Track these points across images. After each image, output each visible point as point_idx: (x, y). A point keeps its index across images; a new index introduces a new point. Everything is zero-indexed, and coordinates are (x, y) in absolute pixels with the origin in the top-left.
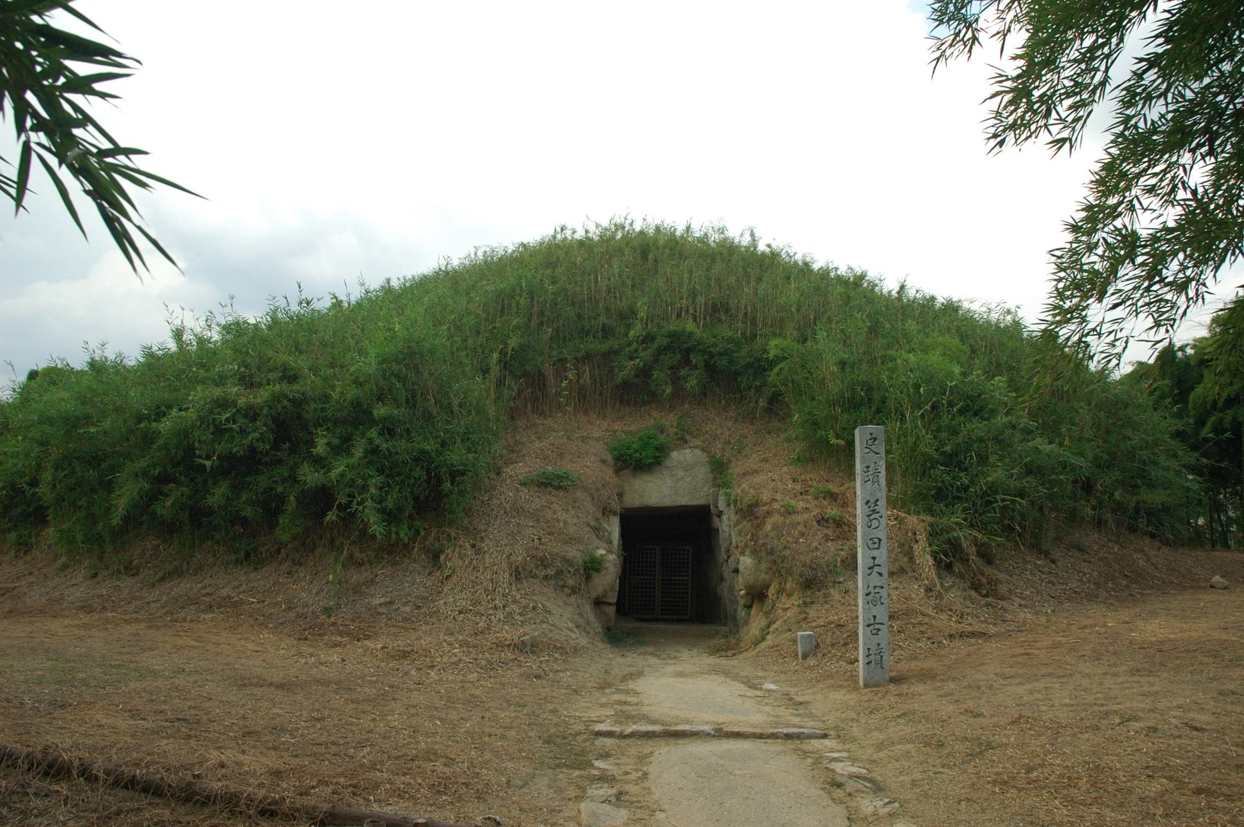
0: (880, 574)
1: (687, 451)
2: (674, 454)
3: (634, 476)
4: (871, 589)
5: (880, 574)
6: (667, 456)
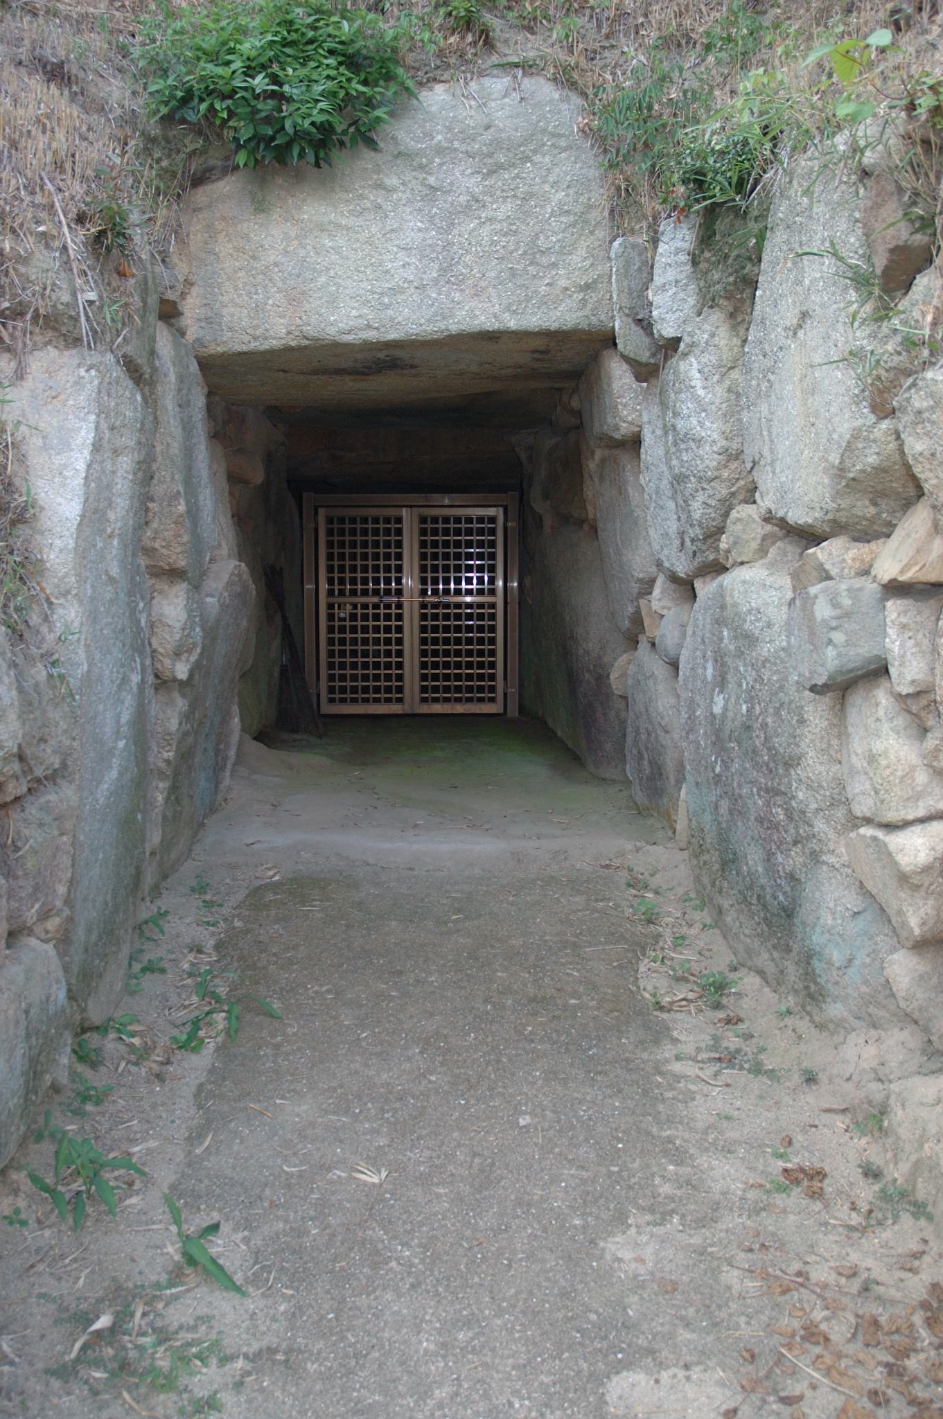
2: (436, 97)
3: (260, 207)
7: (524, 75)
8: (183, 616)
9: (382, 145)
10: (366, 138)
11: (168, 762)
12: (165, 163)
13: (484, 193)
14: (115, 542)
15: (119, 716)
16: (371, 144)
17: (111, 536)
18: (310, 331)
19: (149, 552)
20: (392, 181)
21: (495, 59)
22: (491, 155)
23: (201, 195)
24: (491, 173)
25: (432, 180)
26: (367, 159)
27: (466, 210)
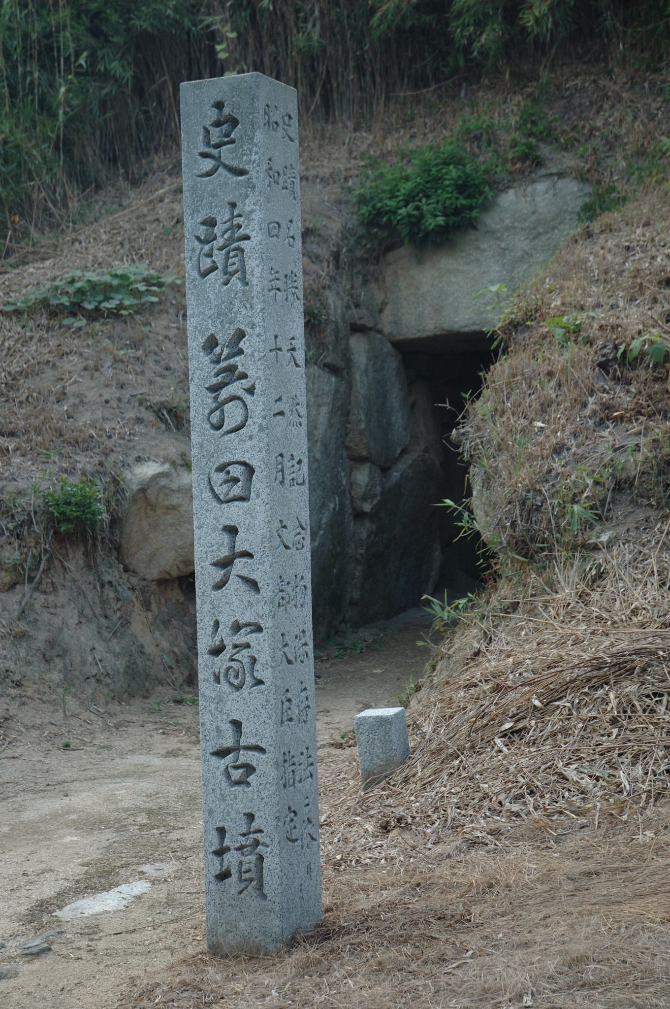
0: (254, 585)
1: (541, 187)
2: (508, 199)
3: (420, 262)
4: (224, 631)
5: (254, 585)
6: (487, 207)
7: (558, 178)
8: (367, 480)
9: (479, 227)
10: (472, 225)
11: (361, 555)
12: (369, 246)
13: (531, 249)
14: (319, 444)
15: (321, 518)
16: (475, 228)
17: (316, 441)
18: (446, 326)
19: (348, 448)
20: (484, 246)
21: (543, 171)
22: (534, 228)
23: (391, 256)
24: (535, 238)
25: (503, 245)
26: (472, 235)
27: (522, 259)
